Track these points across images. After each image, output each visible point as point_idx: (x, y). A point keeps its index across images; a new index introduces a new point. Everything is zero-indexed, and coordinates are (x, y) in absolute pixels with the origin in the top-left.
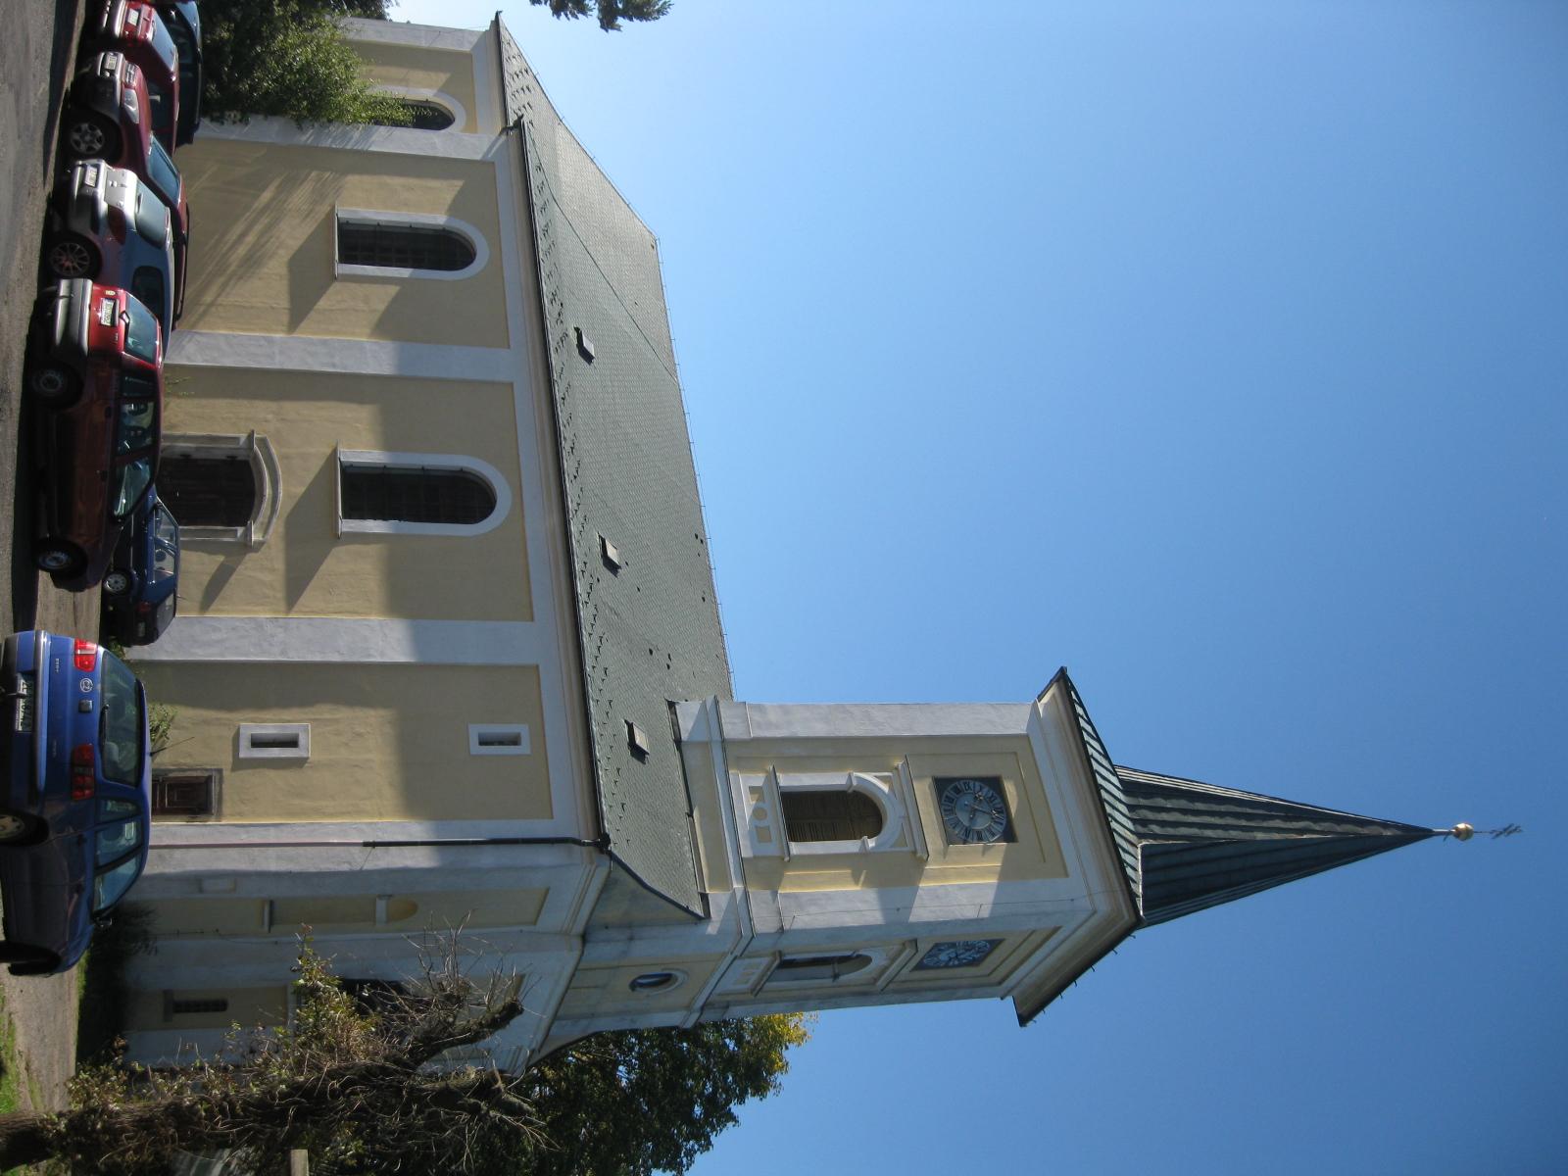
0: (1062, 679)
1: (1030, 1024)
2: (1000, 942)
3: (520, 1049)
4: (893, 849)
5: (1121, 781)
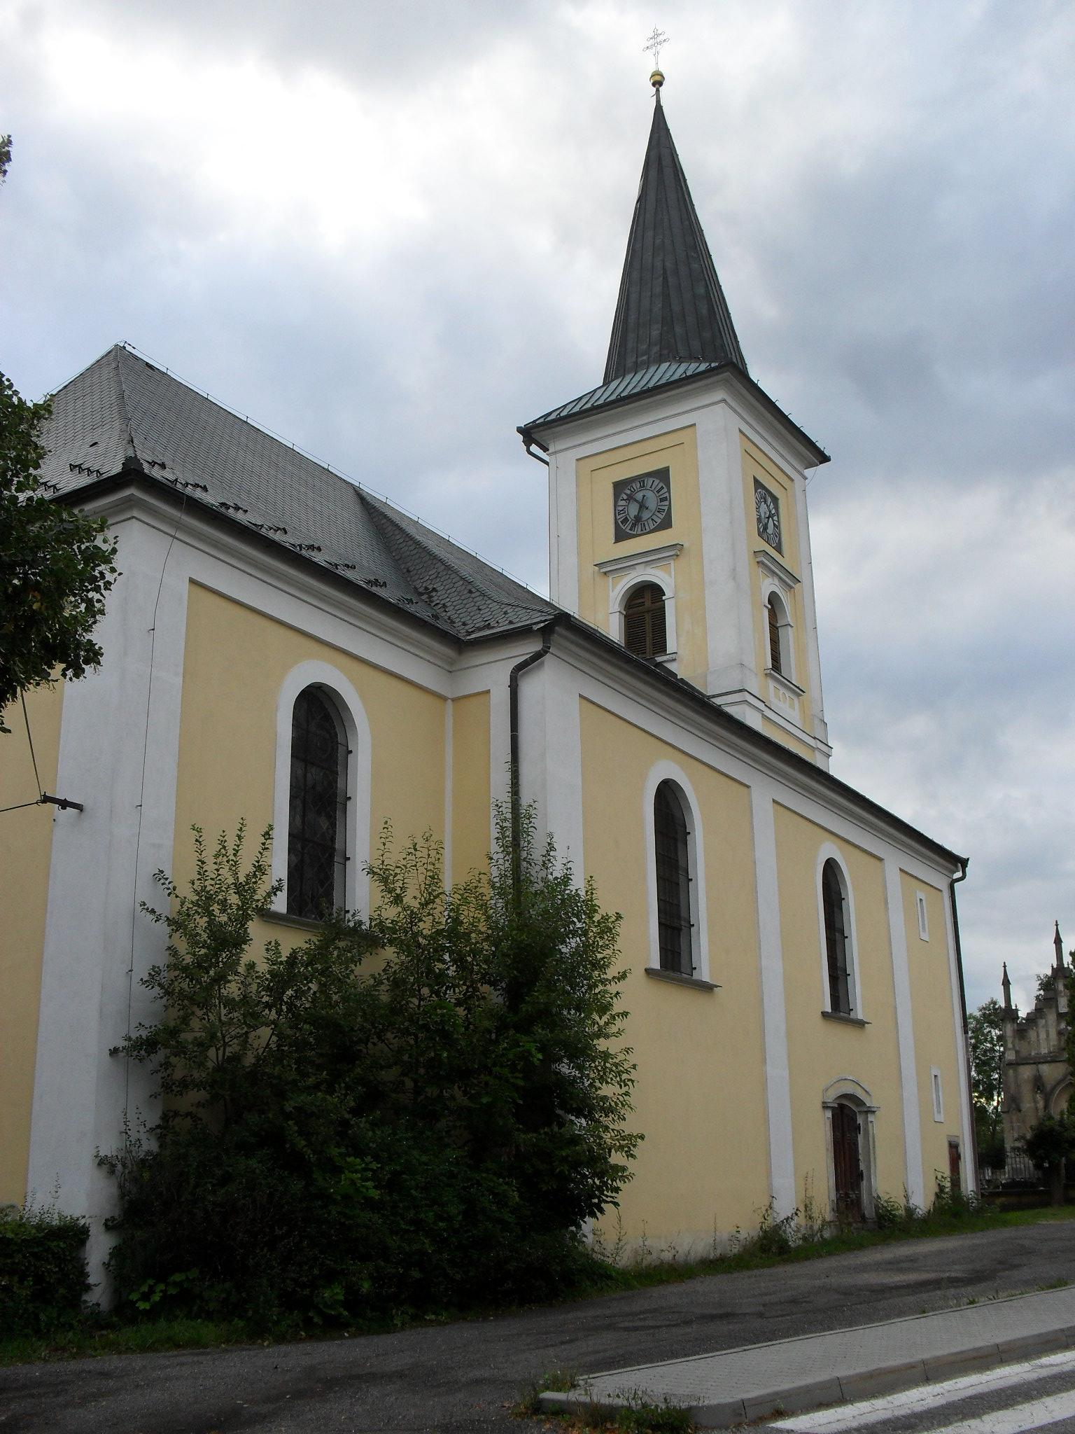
0: (9, 731)
1: (827, 453)
2: (756, 481)
3: (198, 865)
4: (673, 576)
5: (616, 378)
